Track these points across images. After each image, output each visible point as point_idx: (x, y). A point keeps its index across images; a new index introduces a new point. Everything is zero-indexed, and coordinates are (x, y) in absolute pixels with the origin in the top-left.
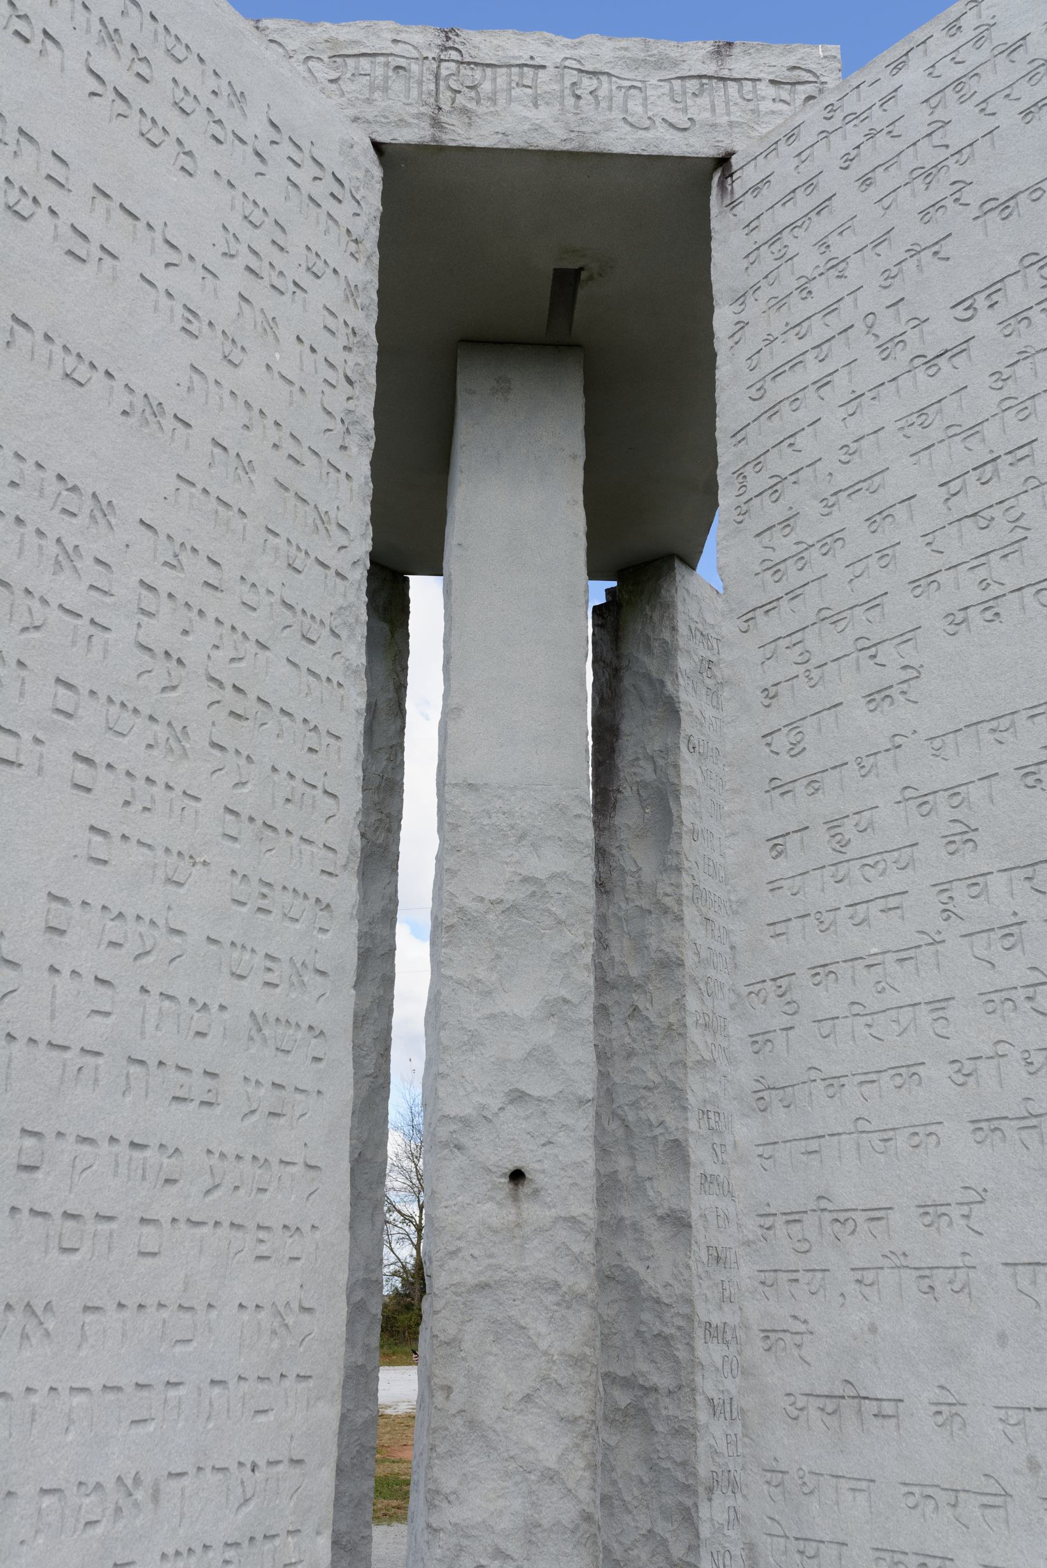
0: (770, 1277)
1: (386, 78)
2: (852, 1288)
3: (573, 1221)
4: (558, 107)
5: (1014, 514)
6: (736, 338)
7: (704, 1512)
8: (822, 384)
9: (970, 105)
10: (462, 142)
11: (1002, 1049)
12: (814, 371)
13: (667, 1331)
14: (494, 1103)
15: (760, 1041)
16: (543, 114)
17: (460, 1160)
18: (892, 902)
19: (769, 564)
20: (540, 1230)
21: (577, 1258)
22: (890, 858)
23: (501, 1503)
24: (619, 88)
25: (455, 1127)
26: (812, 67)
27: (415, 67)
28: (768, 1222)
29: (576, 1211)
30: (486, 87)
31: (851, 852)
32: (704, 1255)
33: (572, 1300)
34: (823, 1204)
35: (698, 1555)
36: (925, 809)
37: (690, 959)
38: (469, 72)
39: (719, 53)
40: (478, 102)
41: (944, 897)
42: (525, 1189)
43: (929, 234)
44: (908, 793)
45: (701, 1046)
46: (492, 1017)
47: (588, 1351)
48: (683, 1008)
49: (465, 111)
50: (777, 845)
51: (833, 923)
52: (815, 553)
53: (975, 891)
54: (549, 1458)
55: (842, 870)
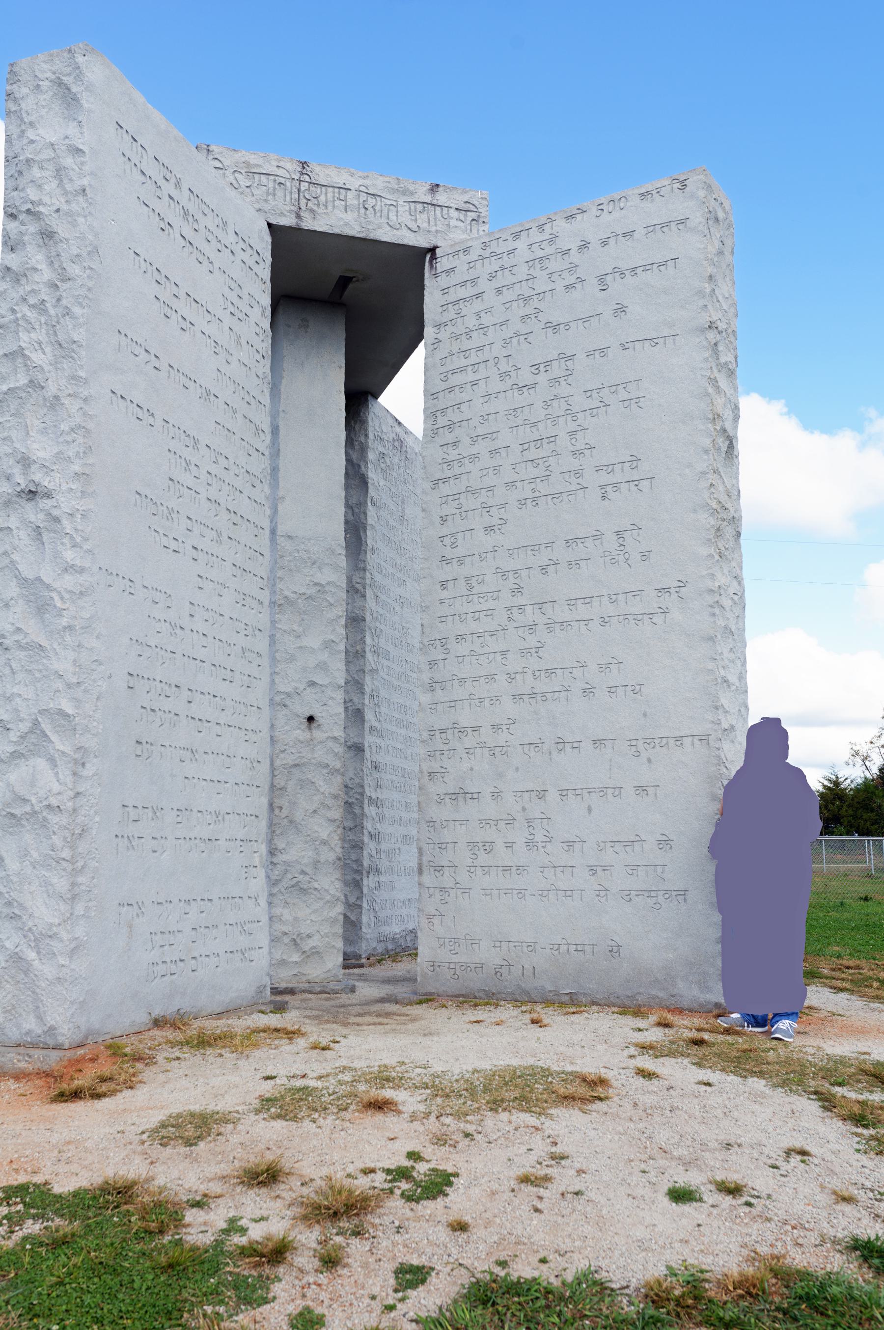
0: (432, 754)
1: (275, 189)
2: (465, 756)
3: (335, 738)
4: (357, 213)
5: (547, 464)
6: (435, 346)
7: (365, 882)
8: (474, 384)
9: (545, 273)
10: (311, 228)
11: (525, 670)
12: (470, 377)
13: (350, 800)
14: (302, 687)
15: (432, 664)
16: (350, 217)
17: (285, 711)
18: (489, 613)
19: (445, 461)
20: (321, 742)
21: (336, 755)
22: (490, 595)
23: (303, 853)
24: (386, 204)
25: (282, 697)
26: (475, 203)
27: (288, 184)
28: (433, 733)
29: (336, 734)
30: (322, 198)
31: (474, 591)
32: (369, 764)
33: (334, 772)
34: (455, 726)
35: (362, 901)
36: (504, 577)
37: (368, 617)
38: (314, 189)
39: (432, 190)
40: (318, 206)
41: (509, 612)
42: (314, 725)
43: (524, 329)
44: (498, 570)
45: (372, 662)
46: (301, 647)
47: (340, 793)
48: (364, 642)
49: (312, 211)
50: (444, 585)
51: (466, 619)
52: (466, 461)
53: (520, 611)
54: (324, 835)
55: (470, 598)
